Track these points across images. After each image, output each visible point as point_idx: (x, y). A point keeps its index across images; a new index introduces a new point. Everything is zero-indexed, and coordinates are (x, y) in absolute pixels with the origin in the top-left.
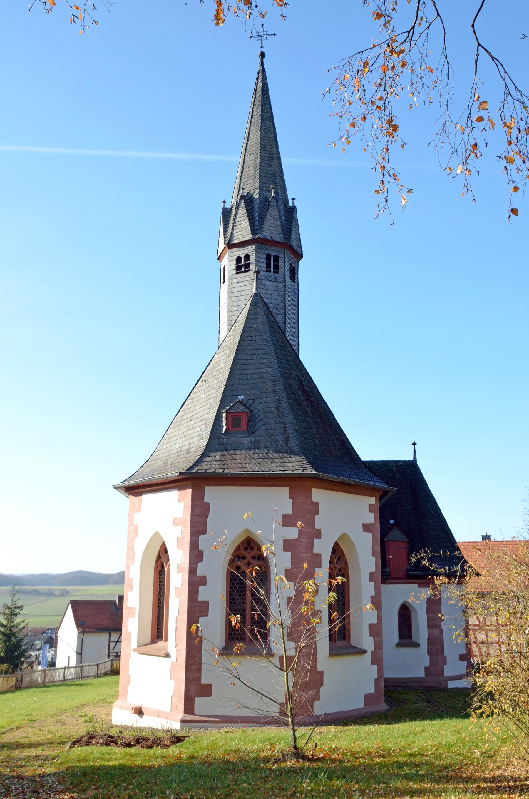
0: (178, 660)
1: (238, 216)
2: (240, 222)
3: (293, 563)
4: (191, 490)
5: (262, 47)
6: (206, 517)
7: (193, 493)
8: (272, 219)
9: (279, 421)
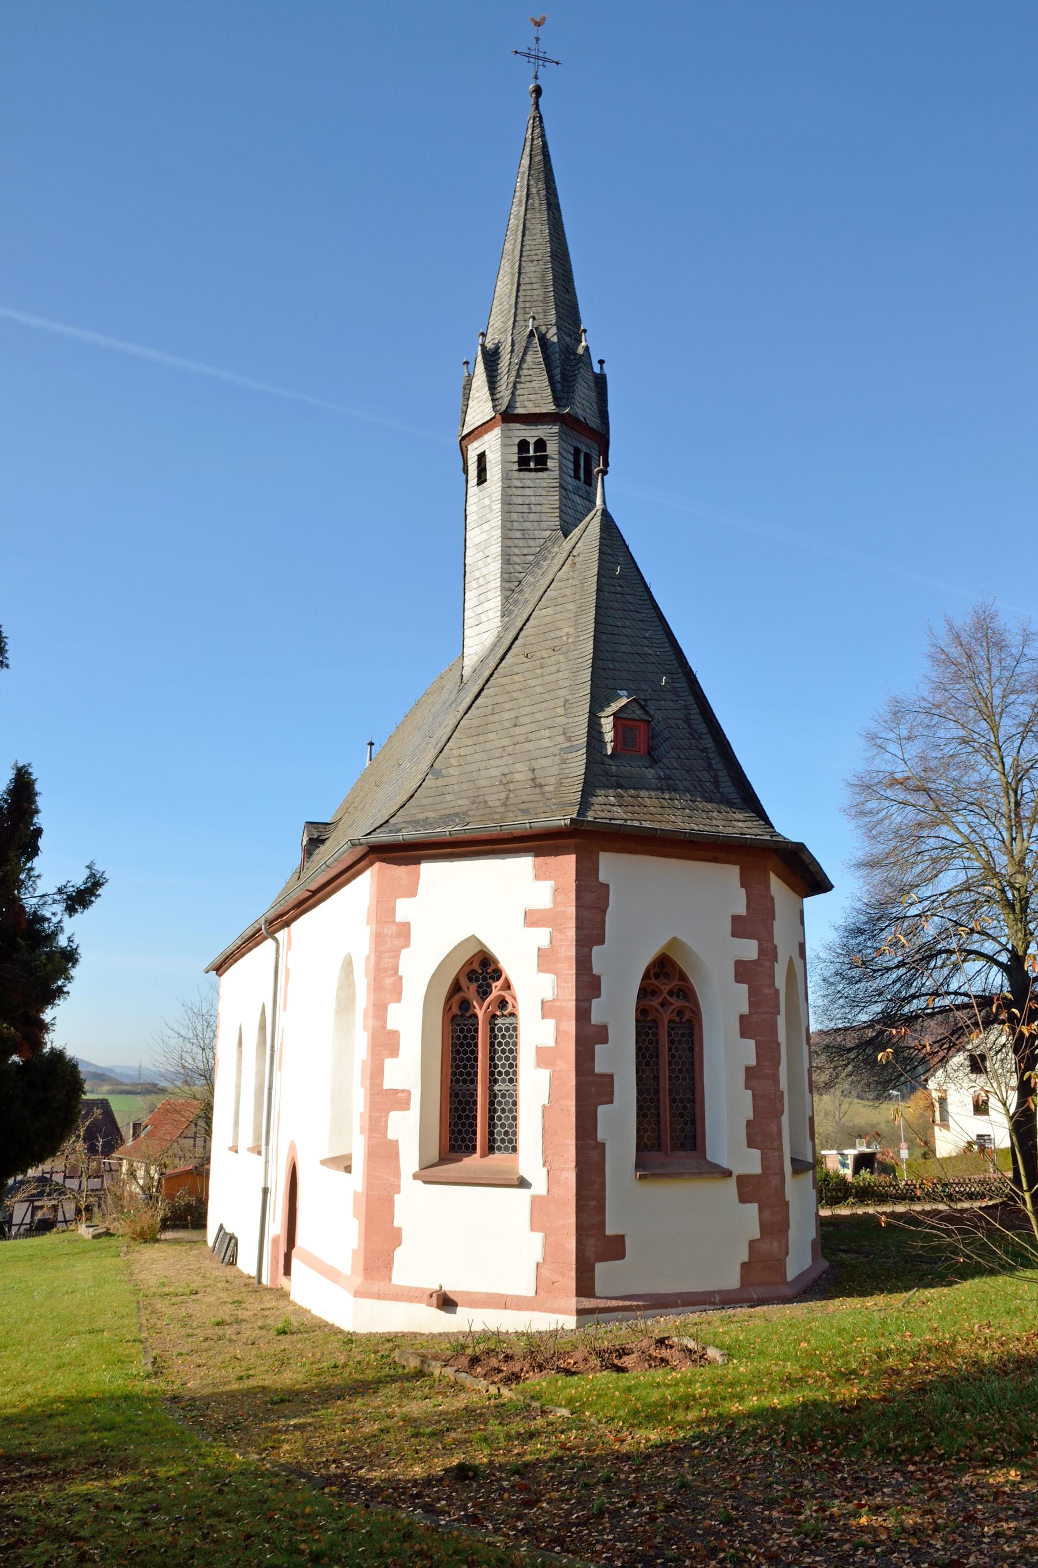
0: (553, 1191)
1: (525, 366)
2: (528, 377)
3: (751, 1004)
4: (573, 857)
5: (536, 78)
6: (603, 910)
7: (578, 862)
8: (586, 386)
9: (696, 746)
